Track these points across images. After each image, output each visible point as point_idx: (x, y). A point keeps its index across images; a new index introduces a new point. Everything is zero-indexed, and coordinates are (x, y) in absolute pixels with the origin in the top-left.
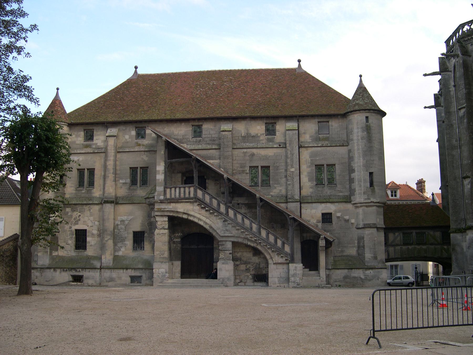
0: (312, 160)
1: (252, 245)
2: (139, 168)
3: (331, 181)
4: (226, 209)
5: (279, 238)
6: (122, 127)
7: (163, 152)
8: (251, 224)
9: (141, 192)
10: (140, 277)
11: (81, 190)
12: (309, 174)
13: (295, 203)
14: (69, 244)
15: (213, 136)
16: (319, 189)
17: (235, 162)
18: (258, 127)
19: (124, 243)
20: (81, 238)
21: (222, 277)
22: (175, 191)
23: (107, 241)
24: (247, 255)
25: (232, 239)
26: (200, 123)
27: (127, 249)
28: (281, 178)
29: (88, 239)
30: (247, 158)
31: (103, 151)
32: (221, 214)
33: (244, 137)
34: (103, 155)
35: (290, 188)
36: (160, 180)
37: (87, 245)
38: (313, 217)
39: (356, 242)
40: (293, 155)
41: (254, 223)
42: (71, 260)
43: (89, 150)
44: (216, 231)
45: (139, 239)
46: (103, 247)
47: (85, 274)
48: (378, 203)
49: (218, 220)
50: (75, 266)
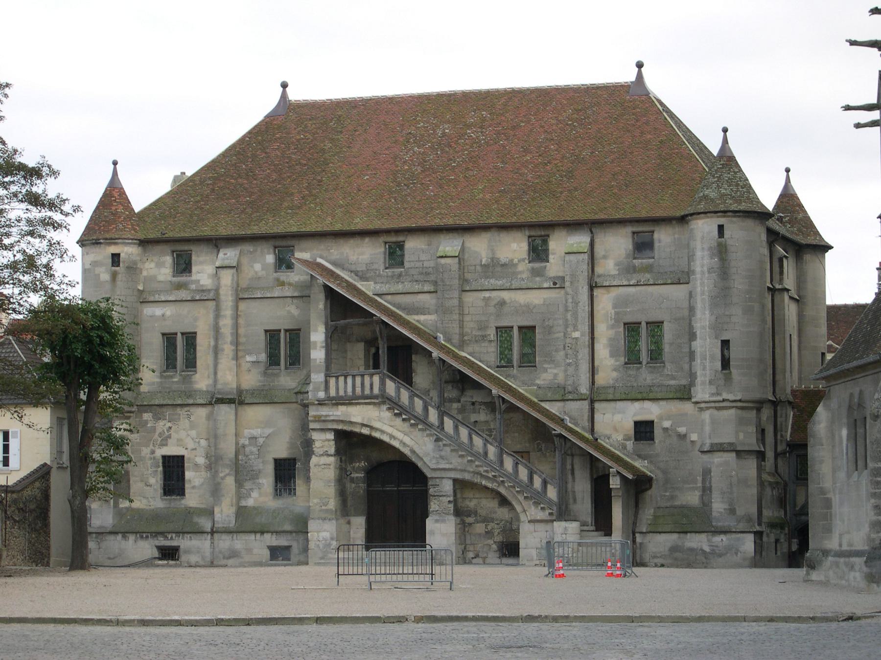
0: (617, 313)
1: (490, 485)
3: (656, 355)
5: (536, 473)
6: (247, 247)
7: (321, 306)
8: (485, 445)
9: (287, 380)
10: (288, 548)
11: (172, 377)
12: (612, 342)
13: (579, 403)
14: (151, 486)
15: (426, 264)
16: (631, 372)
17: (467, 318)
18: (514, 246)
20: (173, 471)
22: (346, 382)
23: (223, 478)
24: (488, 505)
25: (453, 475)
26: (401, 239)
27: (262, 494)
29: (188, 475)
30: (492, 310)
31: (211, 295)
32: (430, 426)
33: (486, 266)
34: (212, 304)
37: (187, 486)
38: (616, 429)
39: (700, 479)
41: (491, 444)
42: (156, 516)
43: (183, 294)
45: (286, 473)
46: (216, 491)
47: (184, 543)
48: (740, 401)
49: (426, 439)
50: (162, 528)
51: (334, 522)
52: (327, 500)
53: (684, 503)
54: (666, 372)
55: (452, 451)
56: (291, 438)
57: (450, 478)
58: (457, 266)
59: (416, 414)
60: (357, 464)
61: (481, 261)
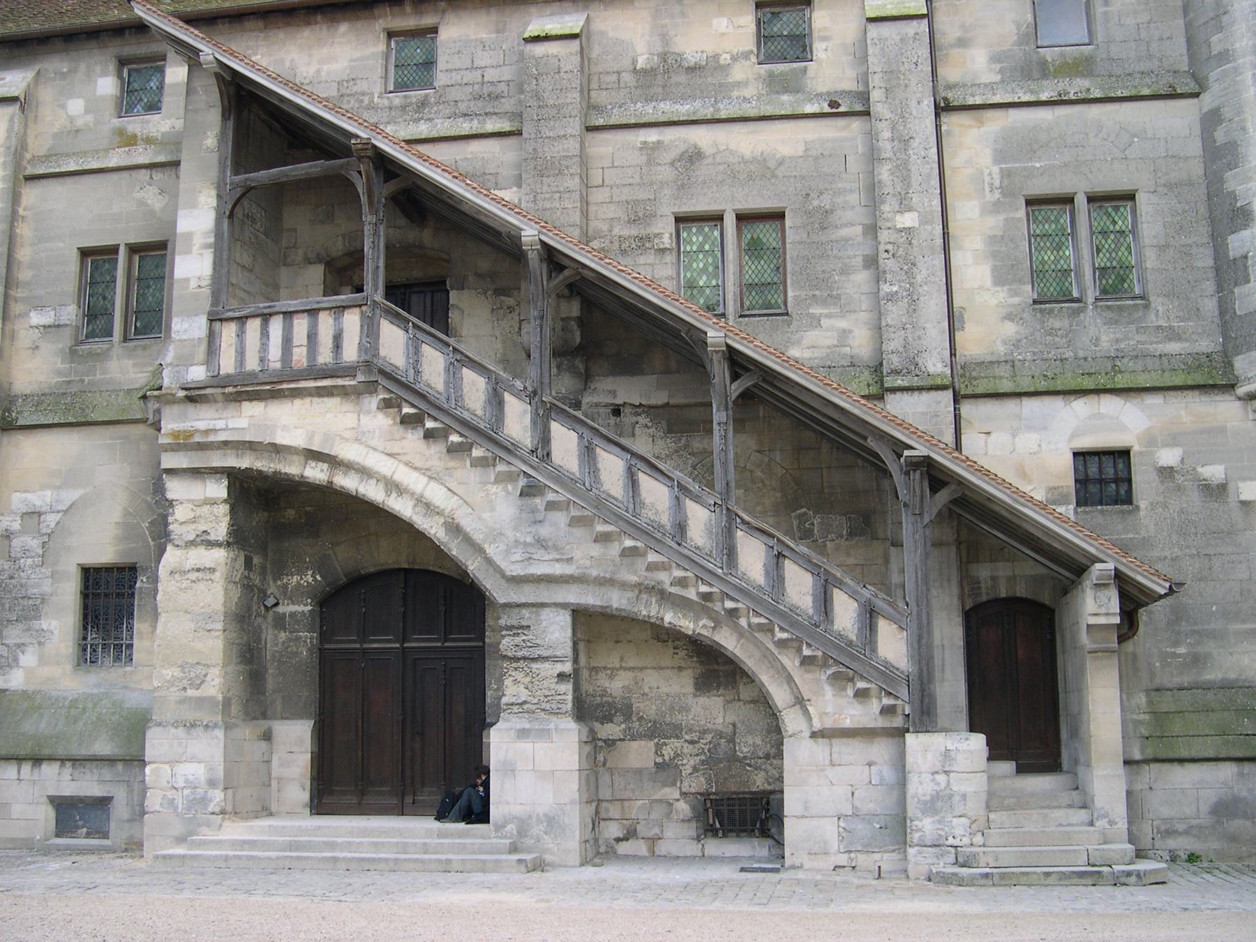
0: (1006, 174)
1: (687, 625)
2: (122, 251)
3: (1116, 284)
4: (534, 422)
5: (840, 584)
10: (103, 803)
12: (997, 246)
13: (926, 397)
15: (490, 75)
17: (598, 196)
18: (721, 24)
19: (36, 624)
21: (517, 810)
22: (265, 334)
24: (665, 687)
26: (427, 21)
28: (842, 273)
30: (665, 173)
32: (510, 449)
33: (645, 76)
35: (894, 314)
36: (193, 284)
40: (906, 142)
41: (697, 499)
44: (480, 550)
49: (493, 489)
51: (220, 733)
52: (200, 670)
53: (1232, 676)
54: (1152, 320)
55: (575, 522)
56: (127, 513)
57: (564, 606)
58: (576, 60)
59: (466, 415)
60: (295, 579)
61: (634, 62)
